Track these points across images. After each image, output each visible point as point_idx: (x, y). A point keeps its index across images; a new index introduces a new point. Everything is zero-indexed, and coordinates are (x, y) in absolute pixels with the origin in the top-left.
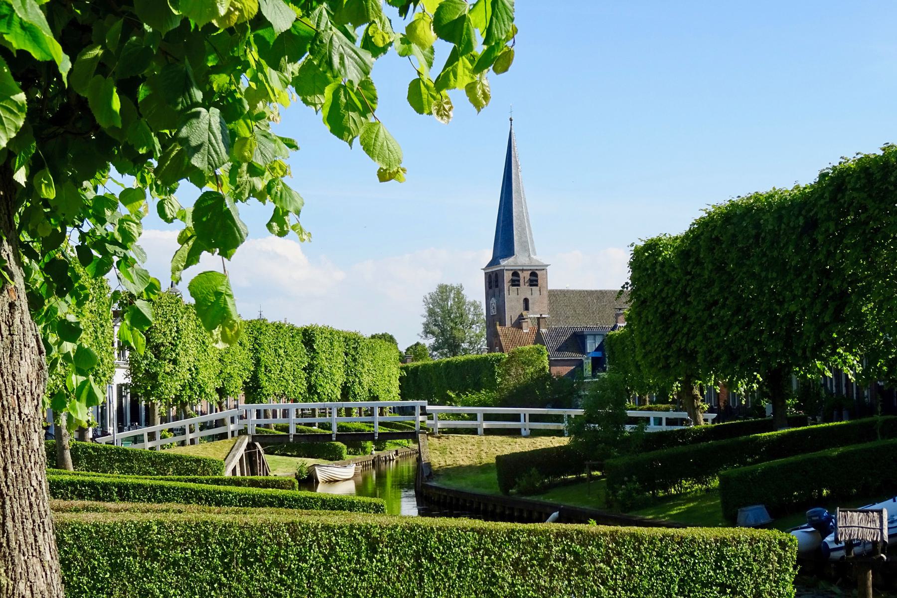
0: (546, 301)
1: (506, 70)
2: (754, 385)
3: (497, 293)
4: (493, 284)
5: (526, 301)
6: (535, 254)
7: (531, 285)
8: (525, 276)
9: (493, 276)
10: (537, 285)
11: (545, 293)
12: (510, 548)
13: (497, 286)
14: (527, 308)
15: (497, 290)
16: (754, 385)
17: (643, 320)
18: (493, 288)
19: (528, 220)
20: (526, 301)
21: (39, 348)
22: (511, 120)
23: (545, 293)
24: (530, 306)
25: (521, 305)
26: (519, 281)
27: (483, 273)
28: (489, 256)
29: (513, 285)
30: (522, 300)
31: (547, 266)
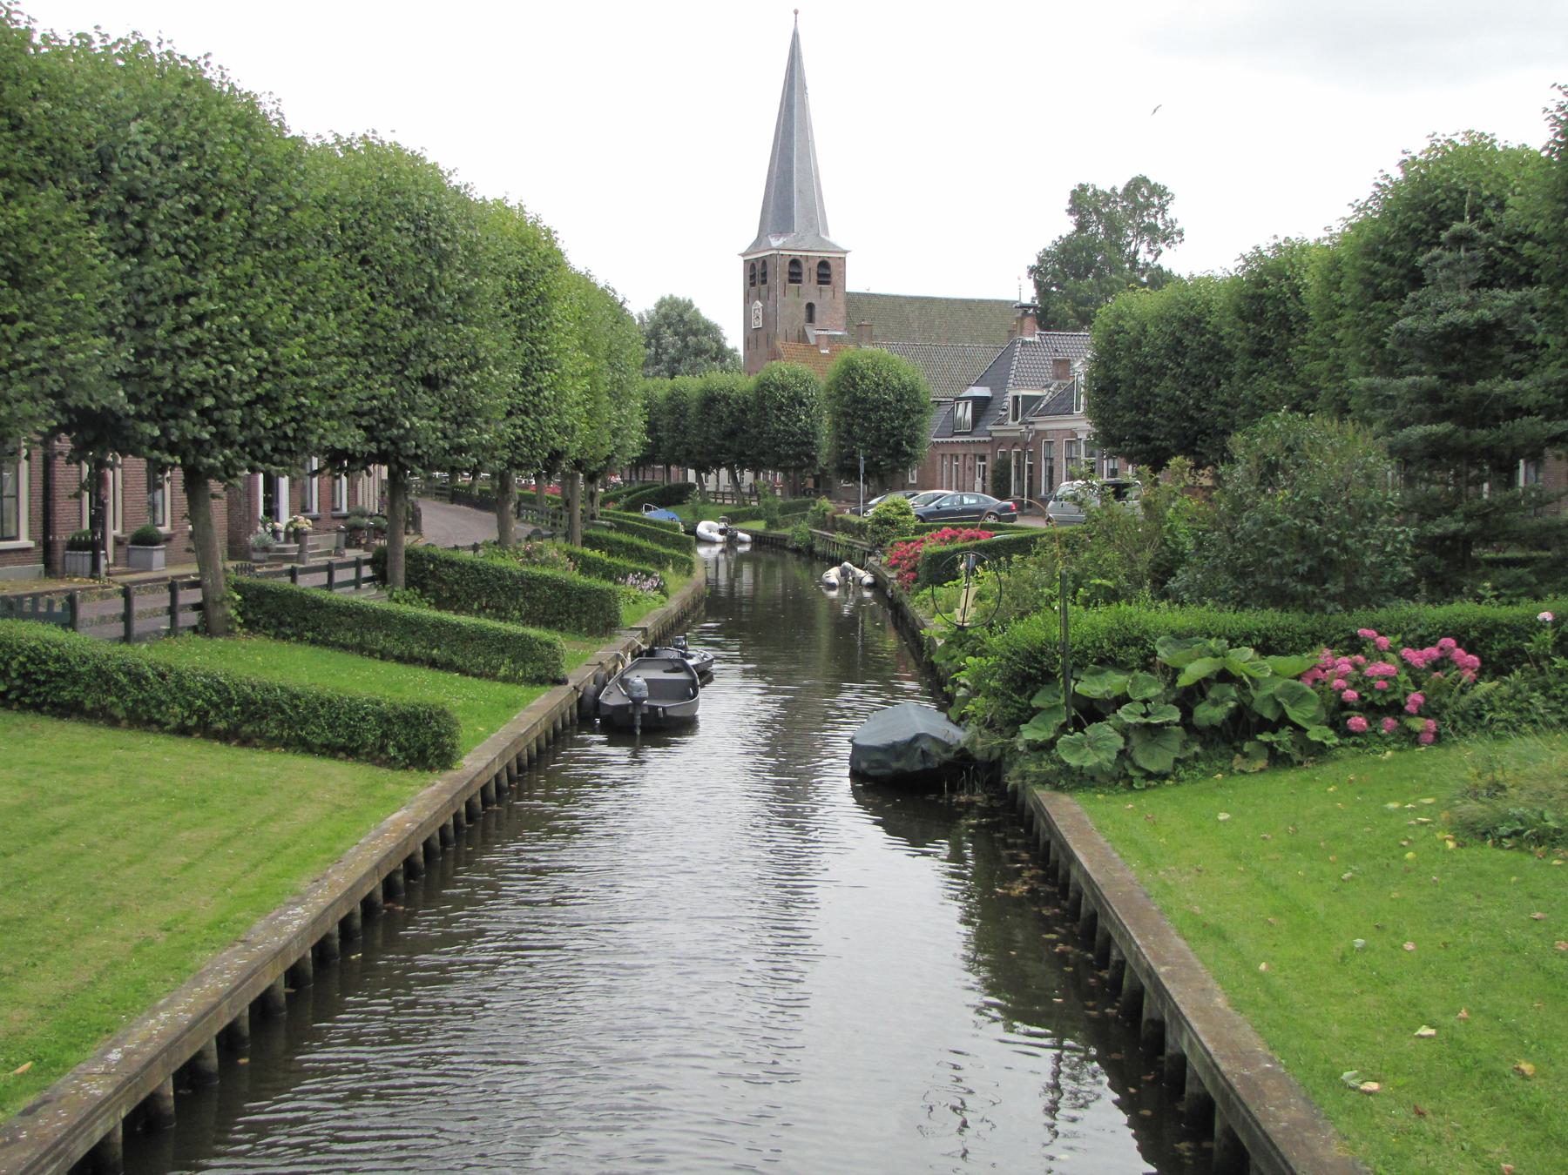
0: (842, 309)
1: (1074, 192)
2: (1368, 562)
3: (764, 293)
4: (758, 278)
5: (810, 307)
7: (820, 283)
8: (809, 272)
9: (759, 266)
10: (828, 283)
11: (840, 299)
12: (49, 269)
13: (764, 282)
14: (811, 319)
15: (764, 287)
16: (1368, 562)
17: (1502, 733)
19: (817, 177)
20: (810, 307)
21: (634, 492)
22: (796, 12)
23: (839, 296)
24: (817, 315)
25: (803, 314)
26: (800, 274)
27: (741, 261)
29: (791, 281)
30: (804, 306)
31: (846, 252)
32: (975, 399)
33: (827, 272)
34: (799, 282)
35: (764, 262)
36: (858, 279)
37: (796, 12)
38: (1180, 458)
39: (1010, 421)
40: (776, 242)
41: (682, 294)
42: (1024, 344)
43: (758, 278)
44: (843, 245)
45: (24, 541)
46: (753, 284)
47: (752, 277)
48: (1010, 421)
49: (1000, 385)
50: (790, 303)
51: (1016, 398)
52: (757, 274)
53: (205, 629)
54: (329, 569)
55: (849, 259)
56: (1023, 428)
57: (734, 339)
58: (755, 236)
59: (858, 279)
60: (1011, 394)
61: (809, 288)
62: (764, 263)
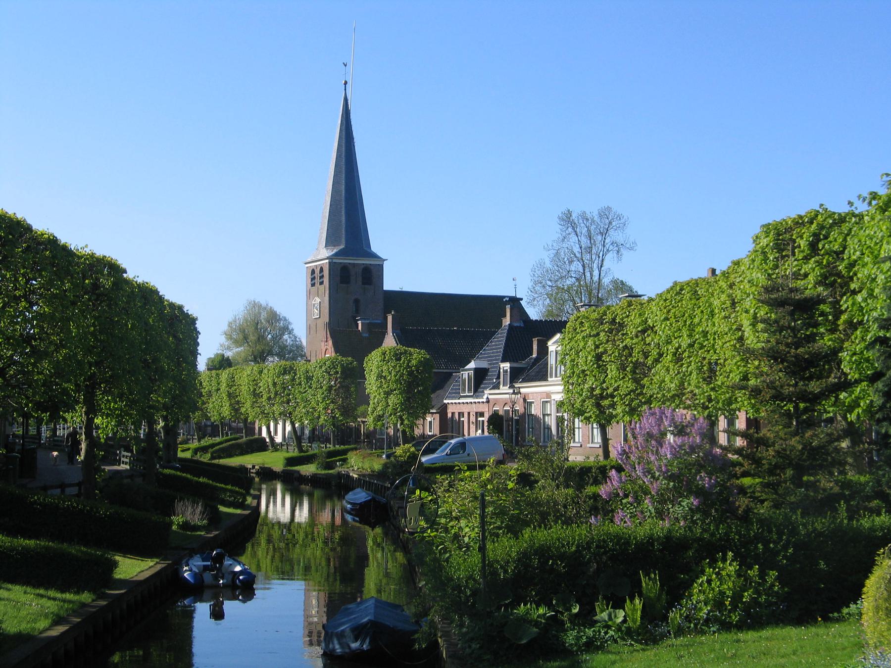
4: (317, 281)
9: (317, 271)
18: (317, 285)
20: (357, 301)
37: (346, 83)
43: (317, 281)
46: (313, 285)
47: (313, 279)
55: (385, 264)
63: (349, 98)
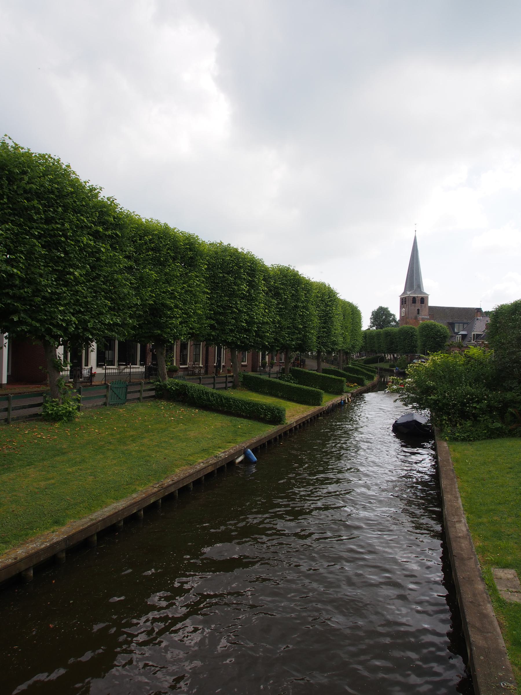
4: (404, 303)
5: (418, 310)
6: (423, 290)
9: (404, 299)
10: (423, 303)
11: (427, 307)
13: (405, 303)
14: (418, 313)
20: (418, 310)
22: (416, 231)
24: (420, 312)
26: (415, 301)
28: (402, 291)
32: (462, 335)
33: (423, 300)
34: (415, 303)
35: (405, 298)
36: (432, 302)
37: (416, 231)
38: (223, 526)
39: (472, 341)
40: (408, 293)
41: (384, 306)
42: (477, 319)
44: (428, 293)
45: (283, 361)
46: (402, 304)
47: (402, 302)
48: (472, 341)
49: (470, 331)
50: (414, 309)
51: (474, 334)
52: (404, 301)
53: (234, 387)
54: (226, 377)
56: (476, 343)
57: (398, 318)
58: (403, 291)
59: (432, 302)
60: (473, 333)
61: (418, 305)
62: (405, 298)
63: (417, 236)
